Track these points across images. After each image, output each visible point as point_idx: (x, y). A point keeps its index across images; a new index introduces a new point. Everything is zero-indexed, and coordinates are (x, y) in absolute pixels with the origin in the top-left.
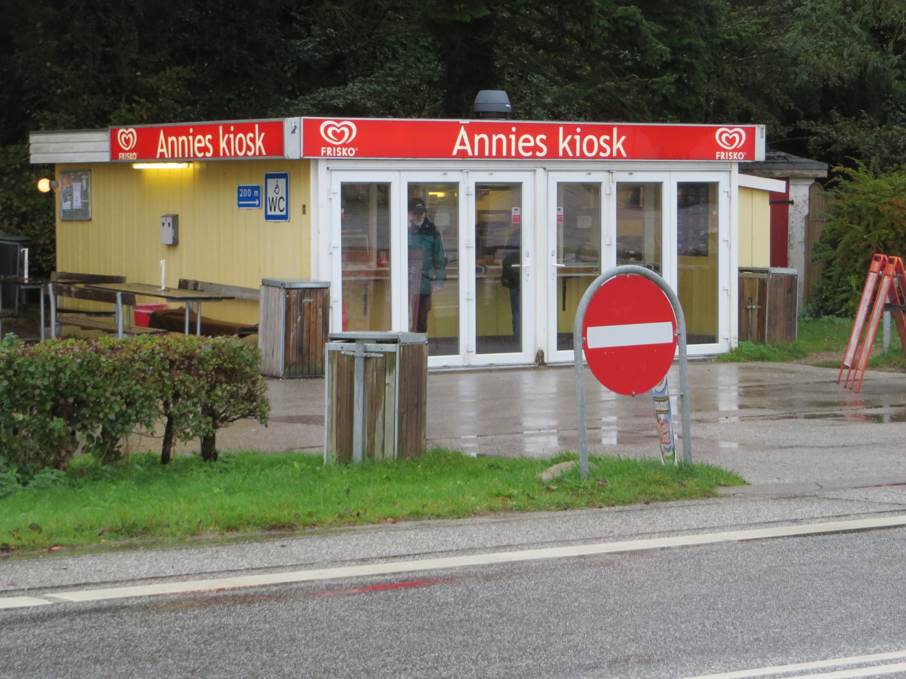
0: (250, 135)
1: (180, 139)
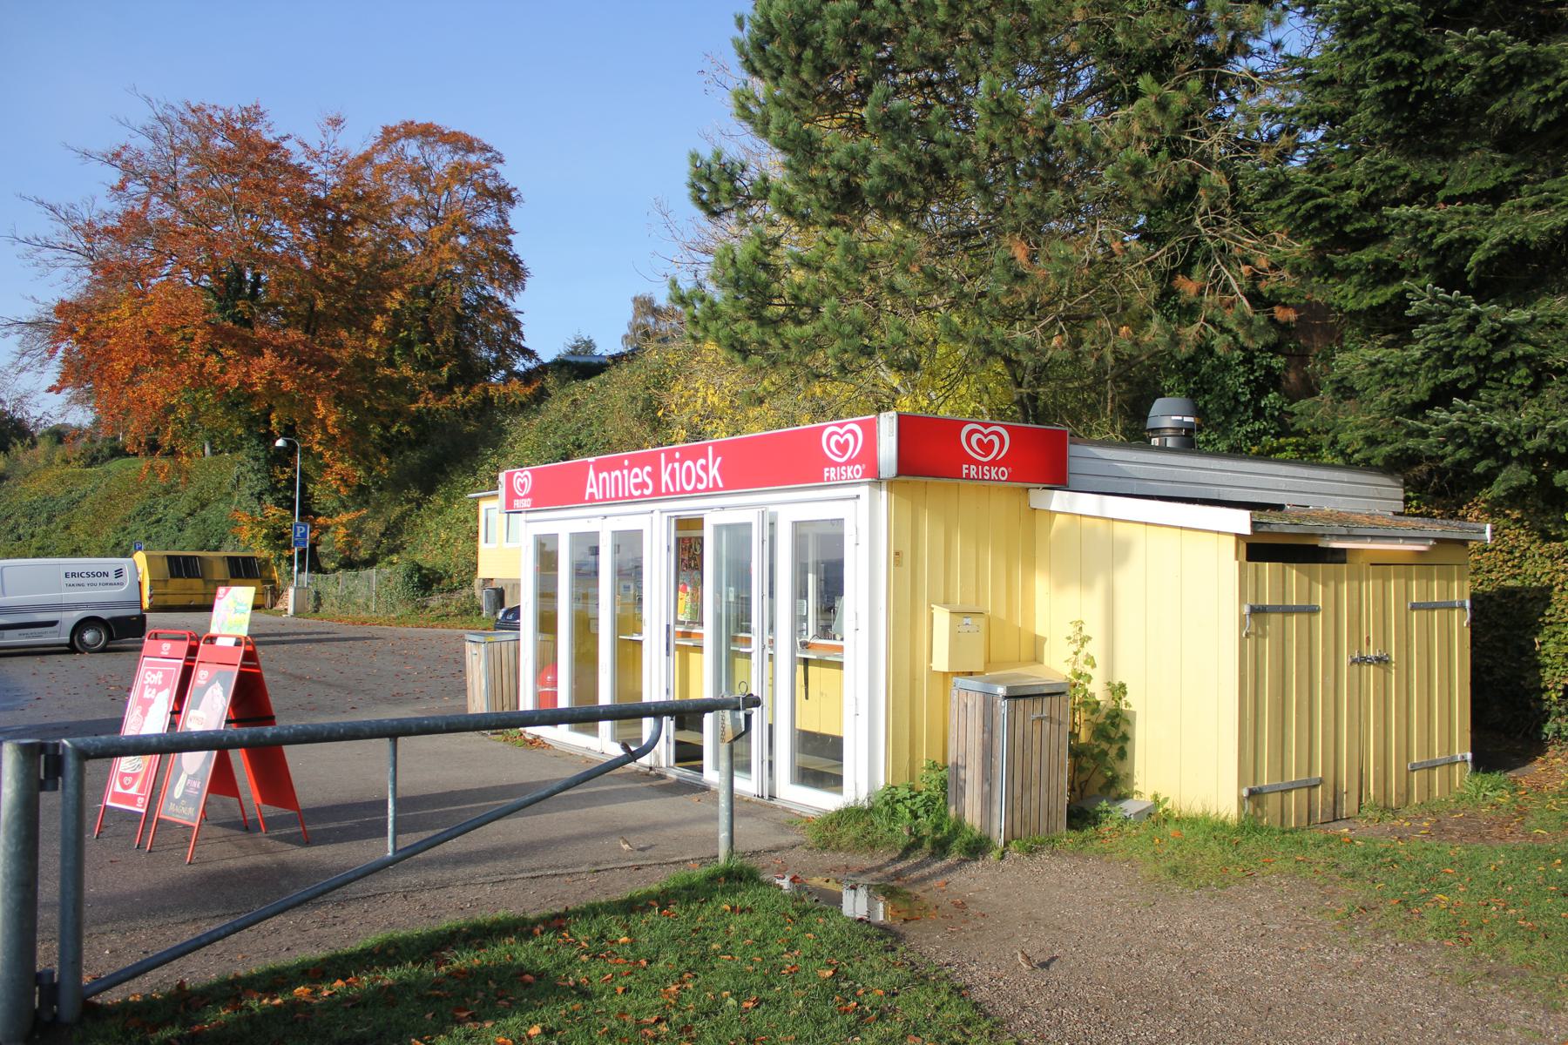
0: (702, 461)
1: (613, 475)
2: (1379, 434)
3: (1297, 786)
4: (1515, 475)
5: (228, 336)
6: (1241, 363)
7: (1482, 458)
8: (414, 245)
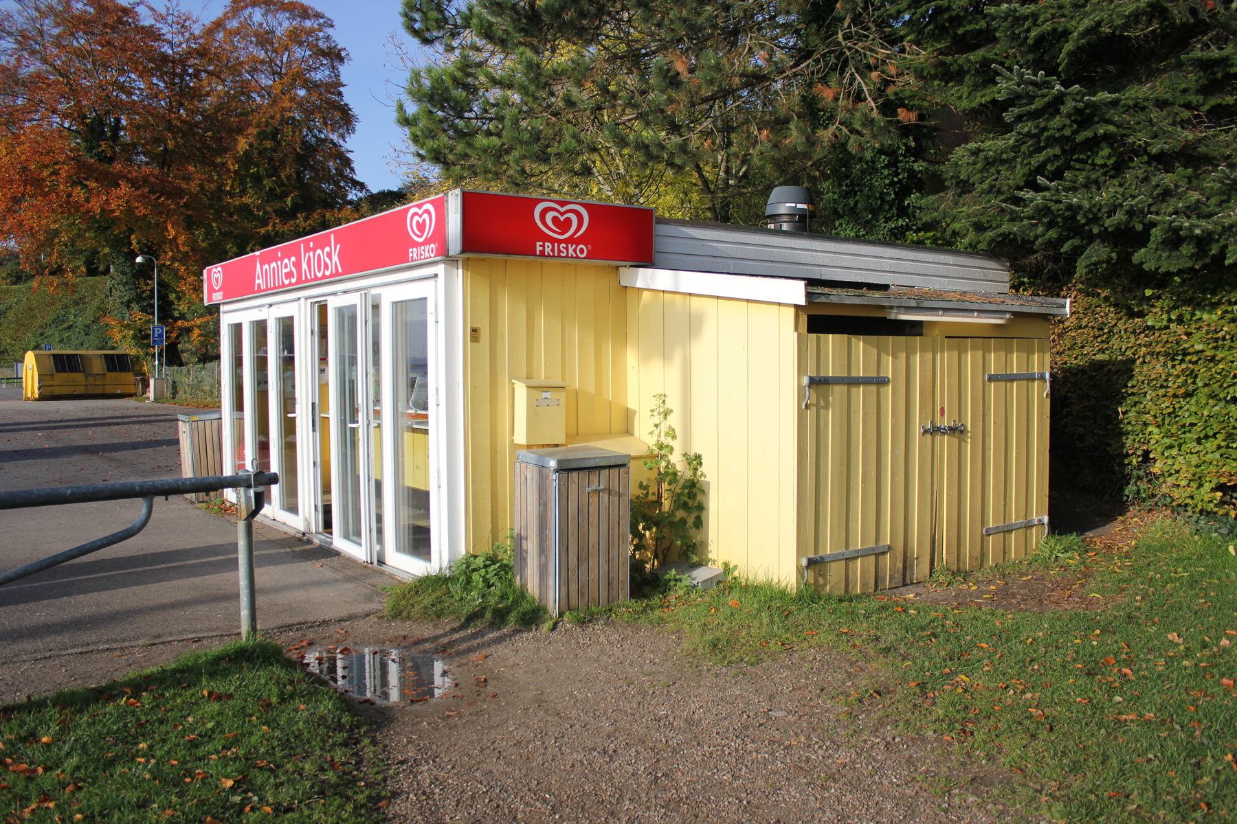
2: (984, 220)
3: (863, 554)
4: (1098, 252)
5: (89, 171)
6: (886, 167)
7: (1068, 238)
8: (262, 97)
